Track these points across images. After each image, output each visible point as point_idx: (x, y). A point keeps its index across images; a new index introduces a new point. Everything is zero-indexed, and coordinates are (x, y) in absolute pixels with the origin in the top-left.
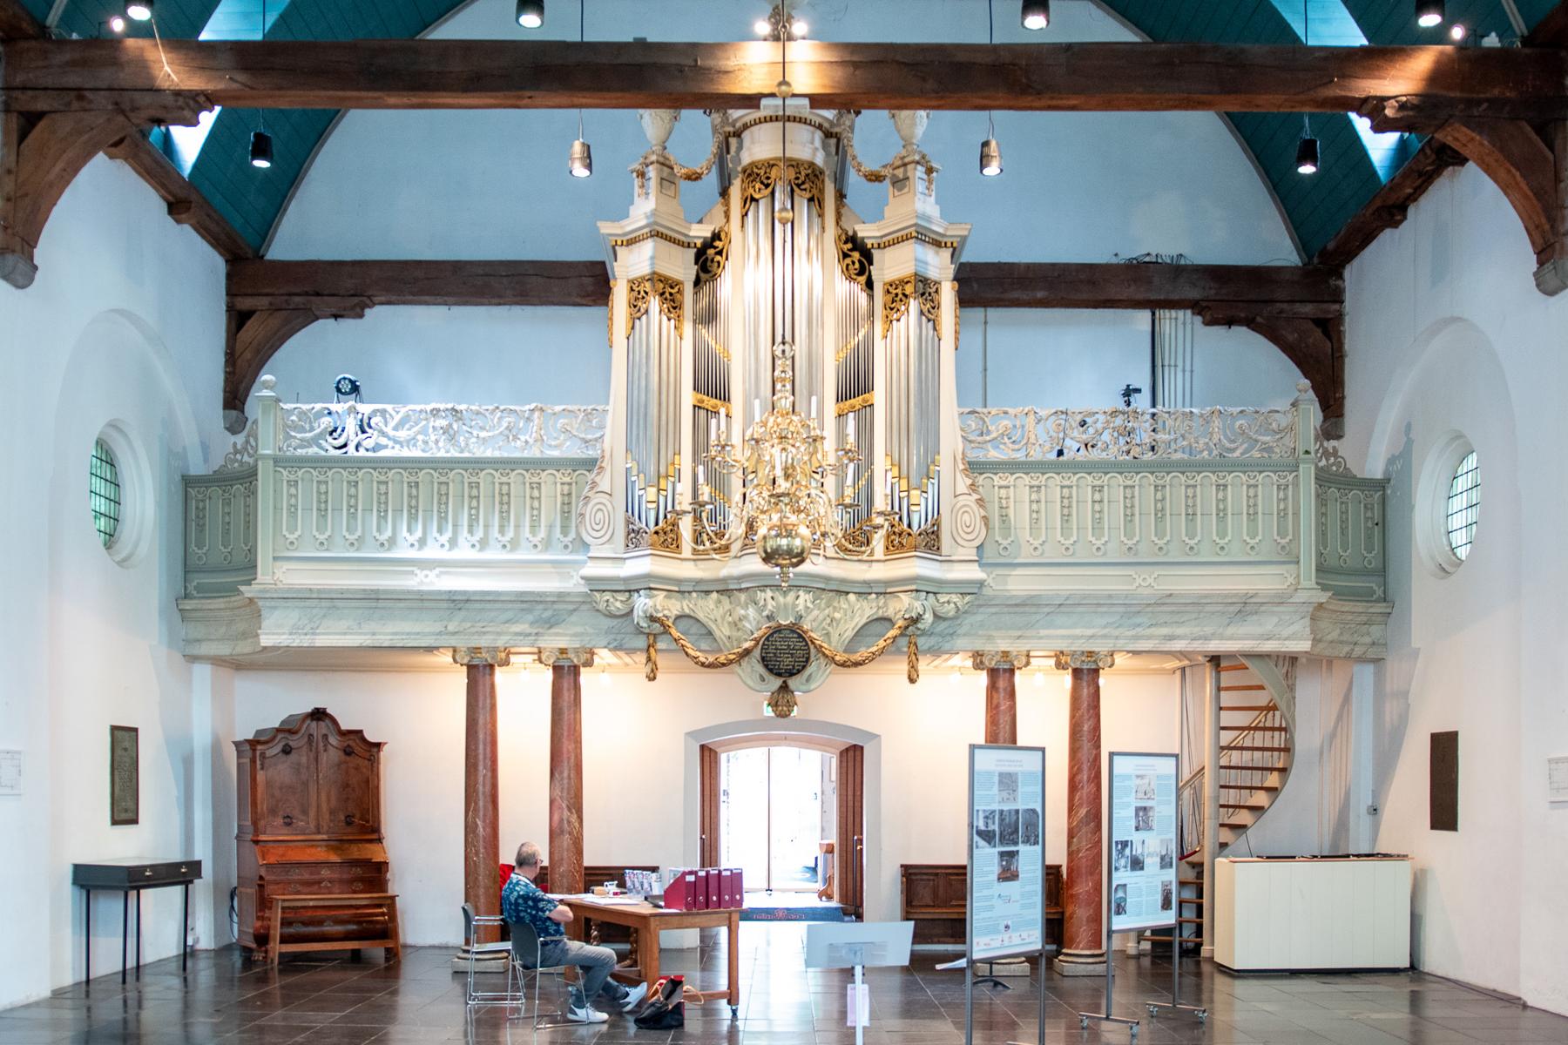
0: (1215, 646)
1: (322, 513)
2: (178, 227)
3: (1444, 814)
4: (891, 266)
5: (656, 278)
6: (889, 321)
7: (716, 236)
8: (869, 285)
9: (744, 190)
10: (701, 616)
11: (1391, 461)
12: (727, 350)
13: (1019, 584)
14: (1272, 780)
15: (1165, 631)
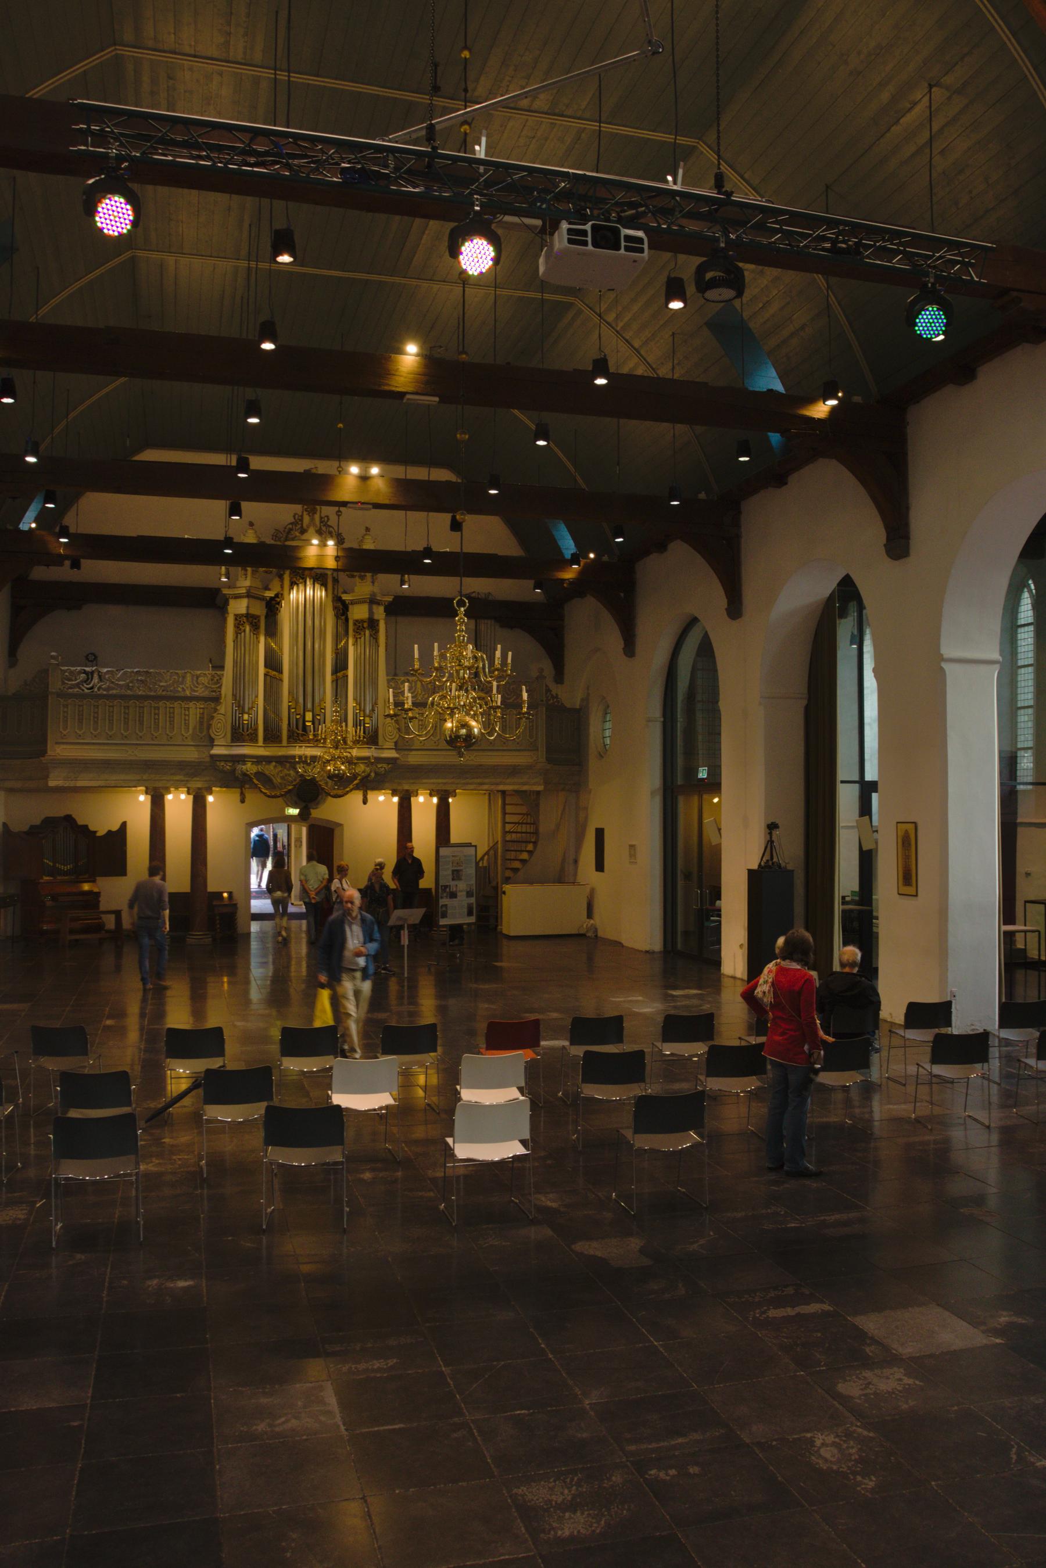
0: (501, 787)
1: (81, 721)
2: (43, 817)
3: (600, 867)
4: (358, 612)
5: (248, 615)
6: (356, 639)
7: (277, 596)
8: (347, 620)
9: (291, 578)
10: (267, 773)
11: (582, 700)
12: (281, 649)
13: (414, 758)
14: (530, 847)
15: (479, 780)
